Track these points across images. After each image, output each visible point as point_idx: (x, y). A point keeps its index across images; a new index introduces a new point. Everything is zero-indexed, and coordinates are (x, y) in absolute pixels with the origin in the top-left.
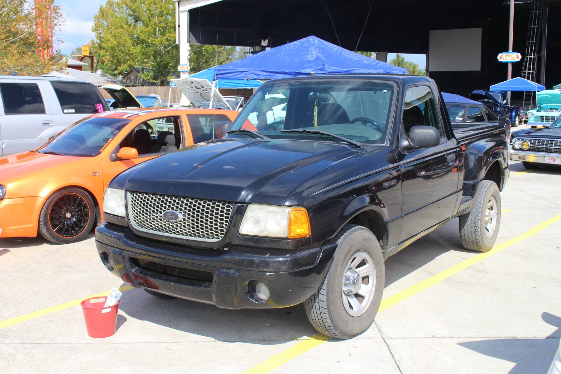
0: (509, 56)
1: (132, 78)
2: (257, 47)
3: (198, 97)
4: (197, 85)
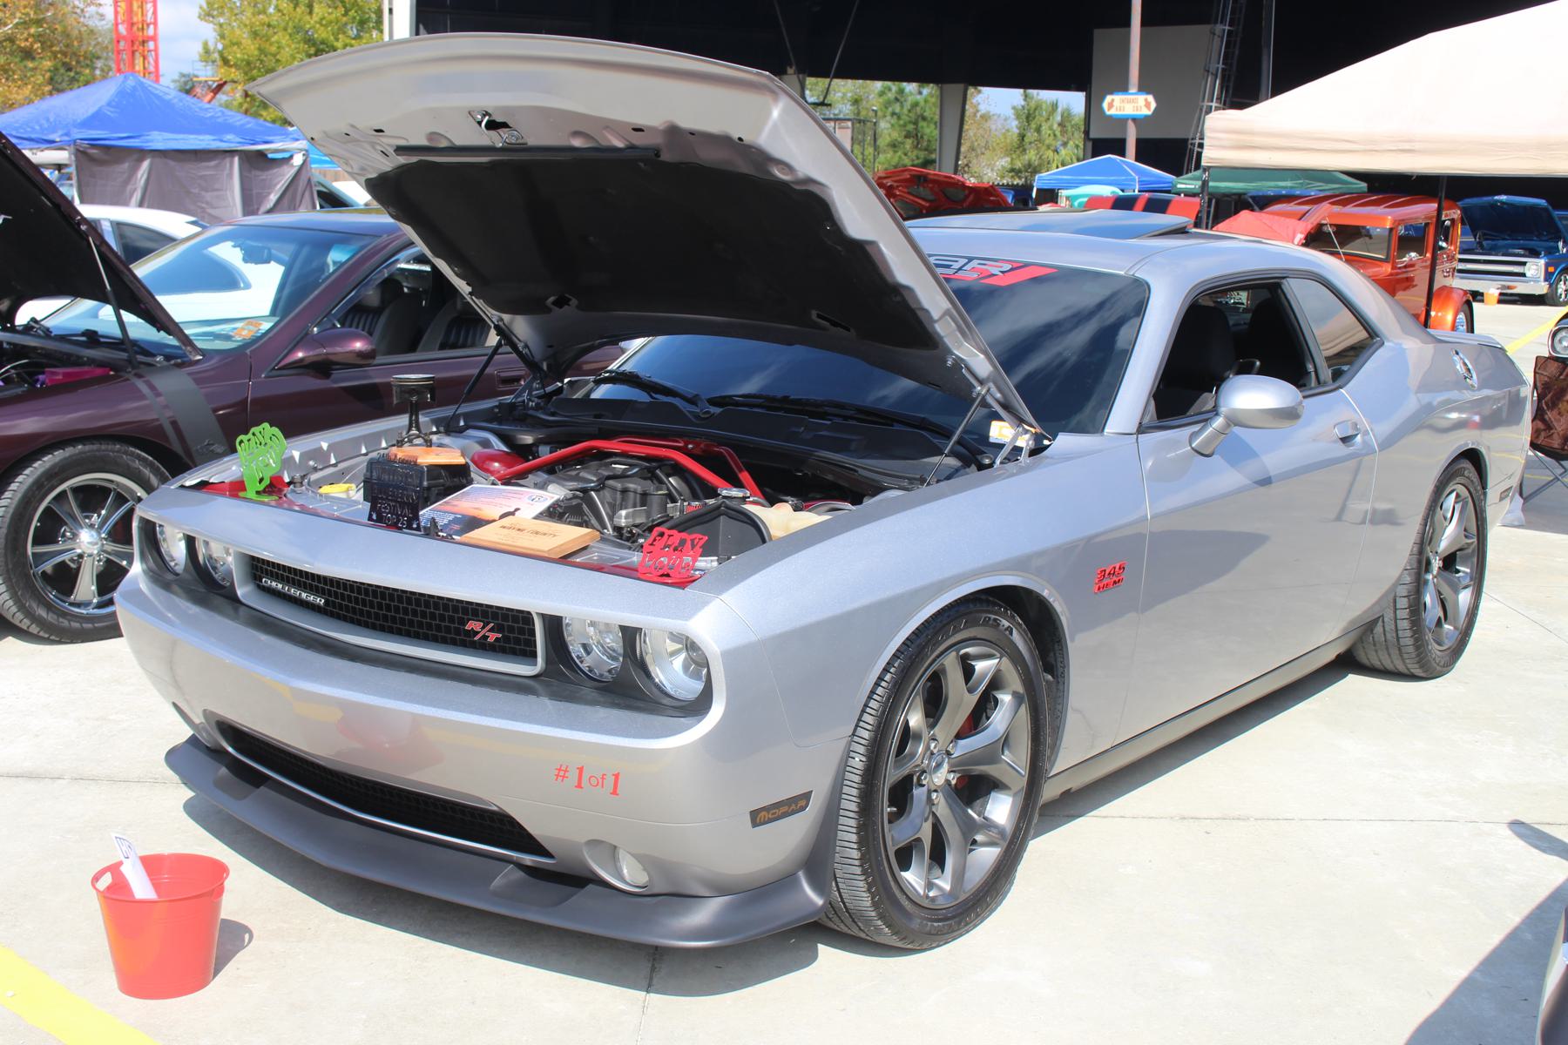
0: (1129, 102)
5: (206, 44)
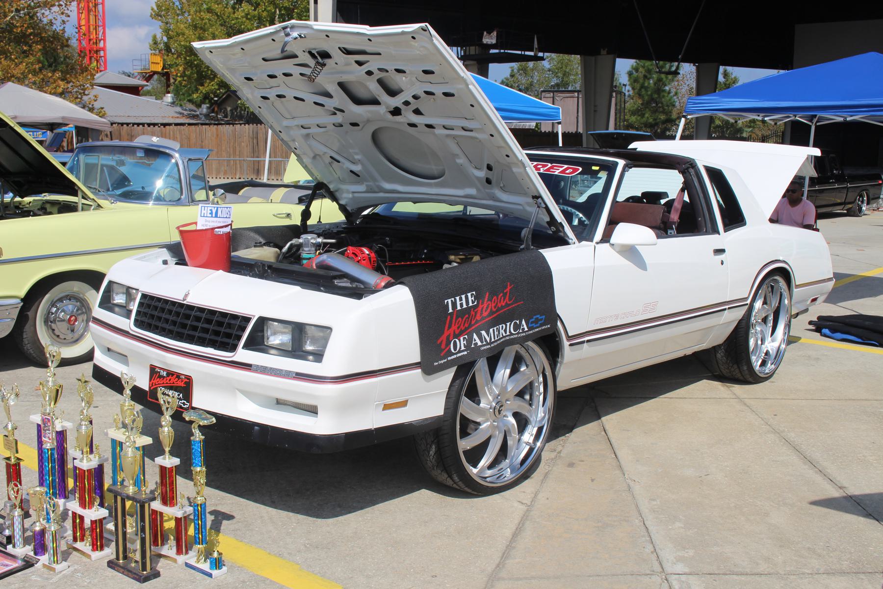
1: (229, 109)
2: (472, 48)
3: (361, 155)
4: (354, 74)
5: (155, 37)
